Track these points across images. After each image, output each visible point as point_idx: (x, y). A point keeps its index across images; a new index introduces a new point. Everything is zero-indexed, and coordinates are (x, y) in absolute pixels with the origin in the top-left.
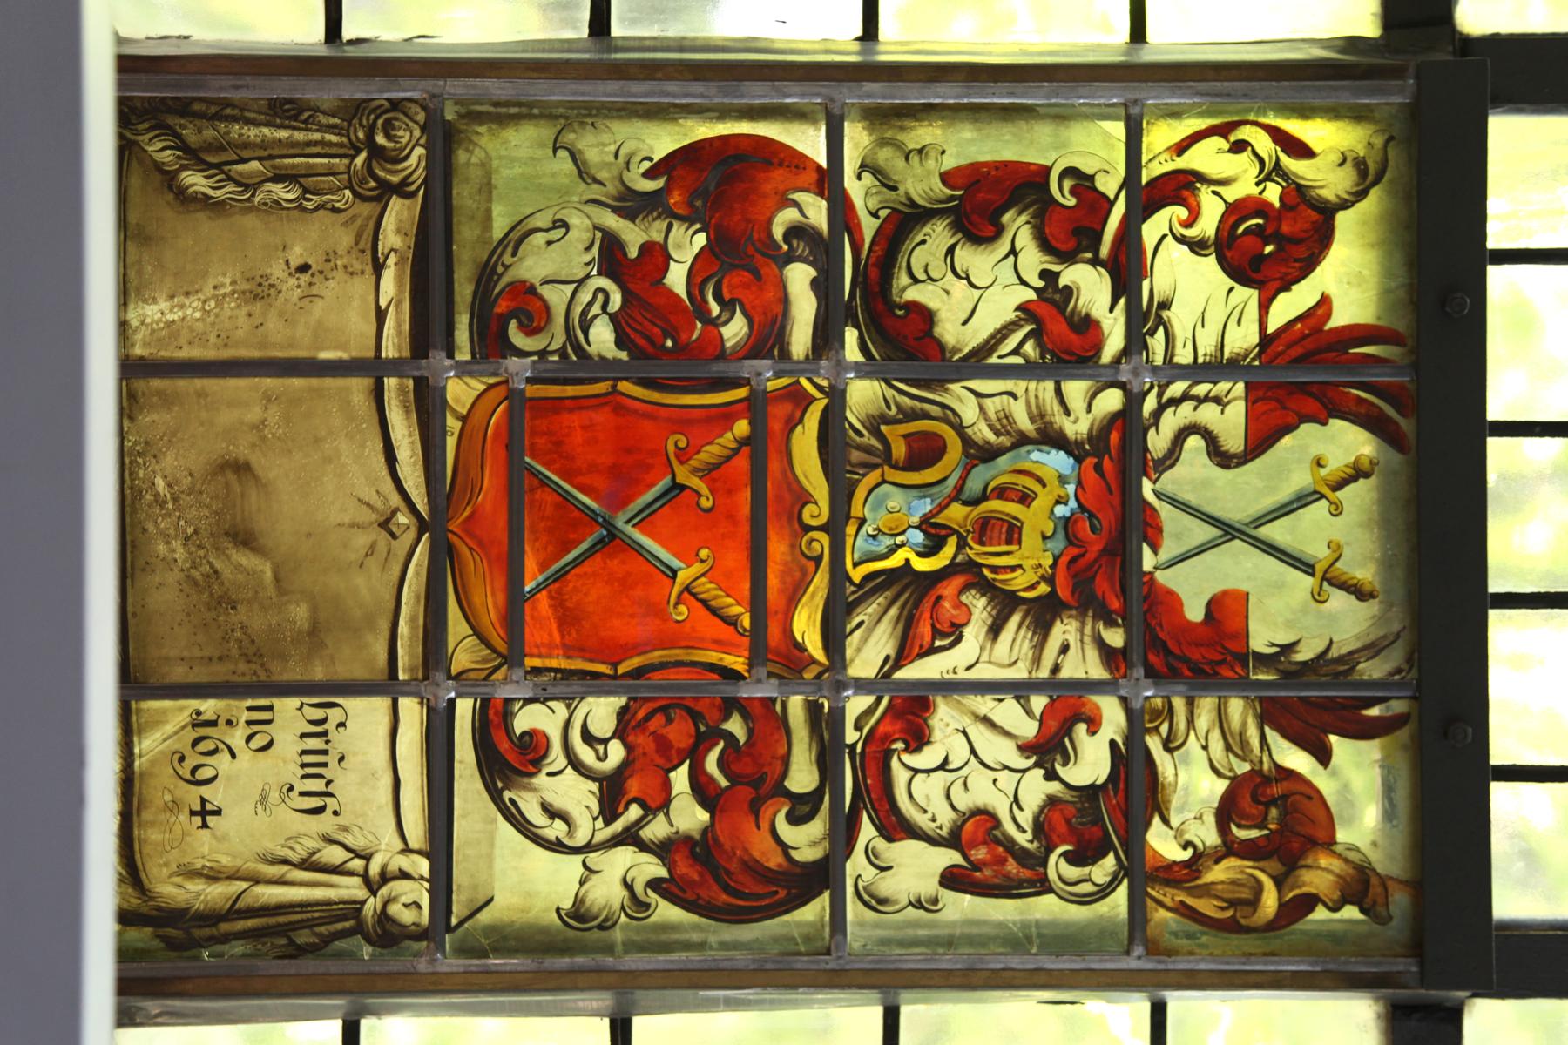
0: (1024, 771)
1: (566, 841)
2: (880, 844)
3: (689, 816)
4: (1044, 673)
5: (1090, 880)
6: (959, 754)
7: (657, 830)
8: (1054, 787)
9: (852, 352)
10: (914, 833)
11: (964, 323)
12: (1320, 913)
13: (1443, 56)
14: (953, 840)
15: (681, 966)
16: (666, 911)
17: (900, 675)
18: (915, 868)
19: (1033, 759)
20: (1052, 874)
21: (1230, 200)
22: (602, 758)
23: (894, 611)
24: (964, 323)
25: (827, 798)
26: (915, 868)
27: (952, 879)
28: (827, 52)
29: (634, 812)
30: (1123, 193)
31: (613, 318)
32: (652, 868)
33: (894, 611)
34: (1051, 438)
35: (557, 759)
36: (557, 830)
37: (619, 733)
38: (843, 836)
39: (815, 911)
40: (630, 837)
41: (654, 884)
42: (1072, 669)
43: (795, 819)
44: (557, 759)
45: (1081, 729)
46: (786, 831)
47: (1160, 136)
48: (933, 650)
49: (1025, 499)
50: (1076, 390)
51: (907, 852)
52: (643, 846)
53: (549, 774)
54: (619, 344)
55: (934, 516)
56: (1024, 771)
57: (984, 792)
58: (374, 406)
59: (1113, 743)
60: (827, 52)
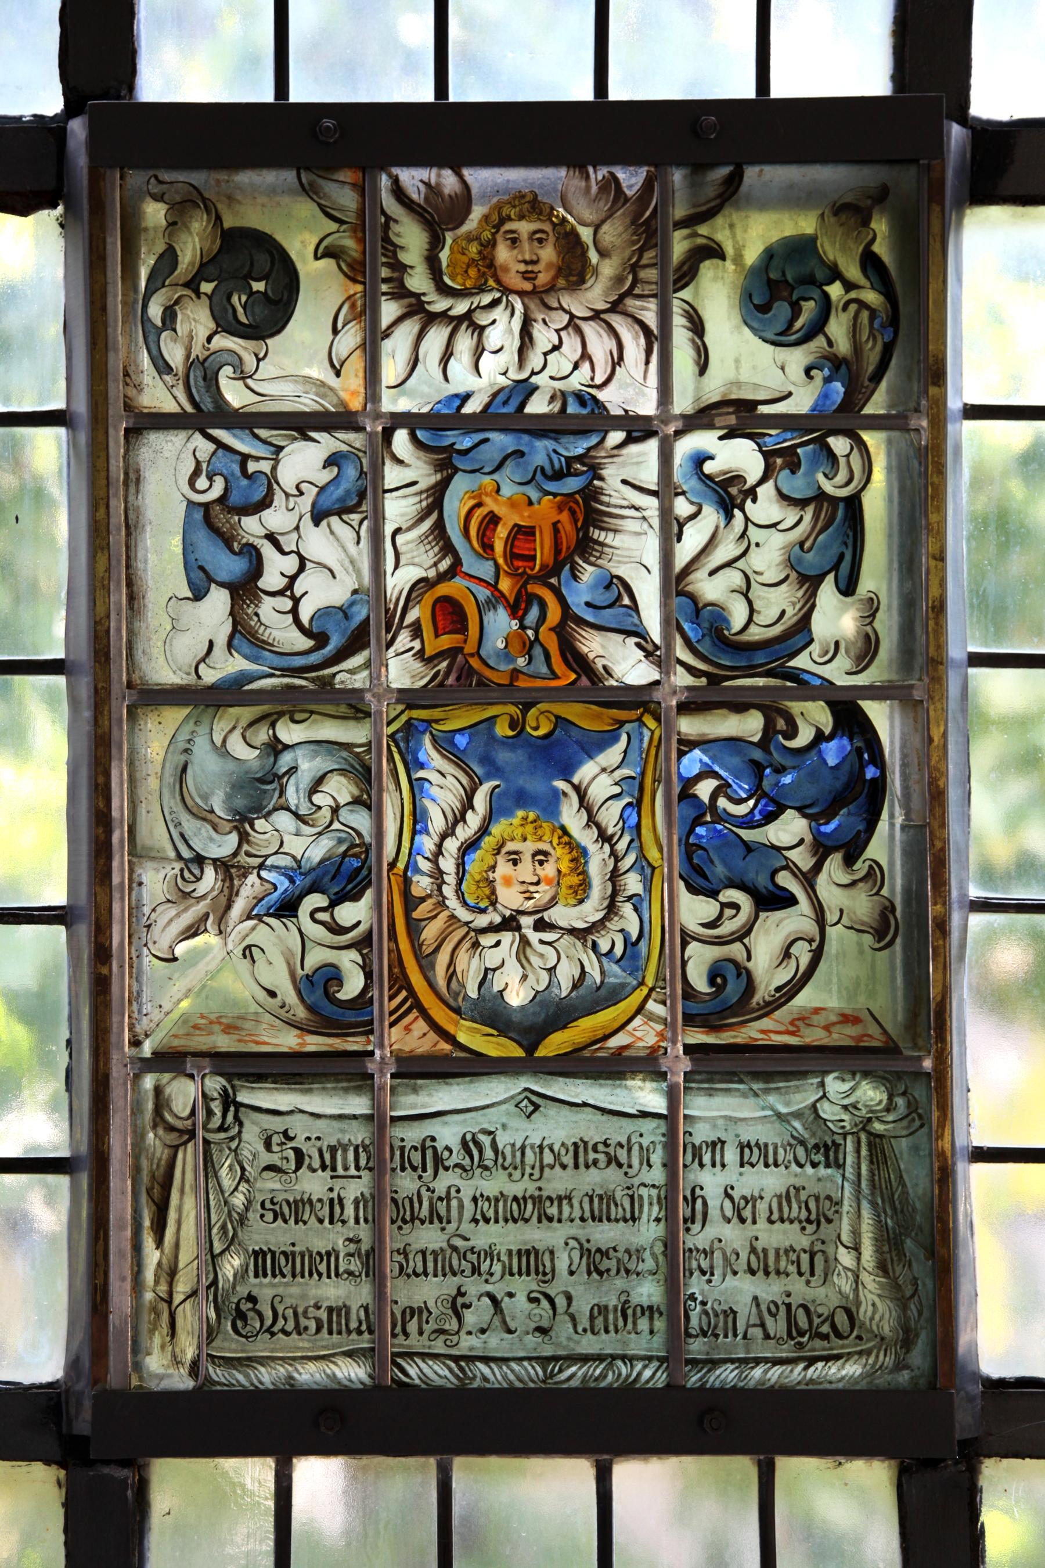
0: (747, 519)
1: (815, 945)
2: (815, 648)
3: (789, 829)
4: (652, 502)
5: (848, 456)
6: (734, 578)
7: (802, 859)
8: (766, 491)
9: (360, 680)
10: (804, 623)
11: (334, 577)
12: (876, 248)
13: (77, 127)
14: (811, 583)
15: (110, 338)
16: (877, 850)
17: (655, 633)
18: (835, 618)
19: (736, 512)
20: (844, 493)
21: (212, 325)
22: (736, 907)
23: (583, 633)
24: (334, 577)
25: (143, 284)
26: (835, 618)
27: (848, 588)
28: (893, 980)
29: (784, 879)
30: (217, 433)
31: (333, 904)
32: (834, 864)
33: (583, 633)
34: (436, 497)
35: (736, 950)
36: (803, 953)
37: (713, 894)
38: (804, 686)
39: (879, 714)
40: (808, 879)
41: (849, 861)
42: (650, 477)
43: (792, 732)
44: (736, 950)
45: (709, 467)
46: (804, 737)
47: (159, 396)
48: (635, 607)
49: (493, 520)
50: (393, 475)
51: (821, 625)
52: (817, 868)
53: (749, 959)
54: (356, 897)
55: (507, 601)
56: (747, 519)
57: (768, 558)
58: (427, 1121)
59: (721, 438)
60: (893, 980)
